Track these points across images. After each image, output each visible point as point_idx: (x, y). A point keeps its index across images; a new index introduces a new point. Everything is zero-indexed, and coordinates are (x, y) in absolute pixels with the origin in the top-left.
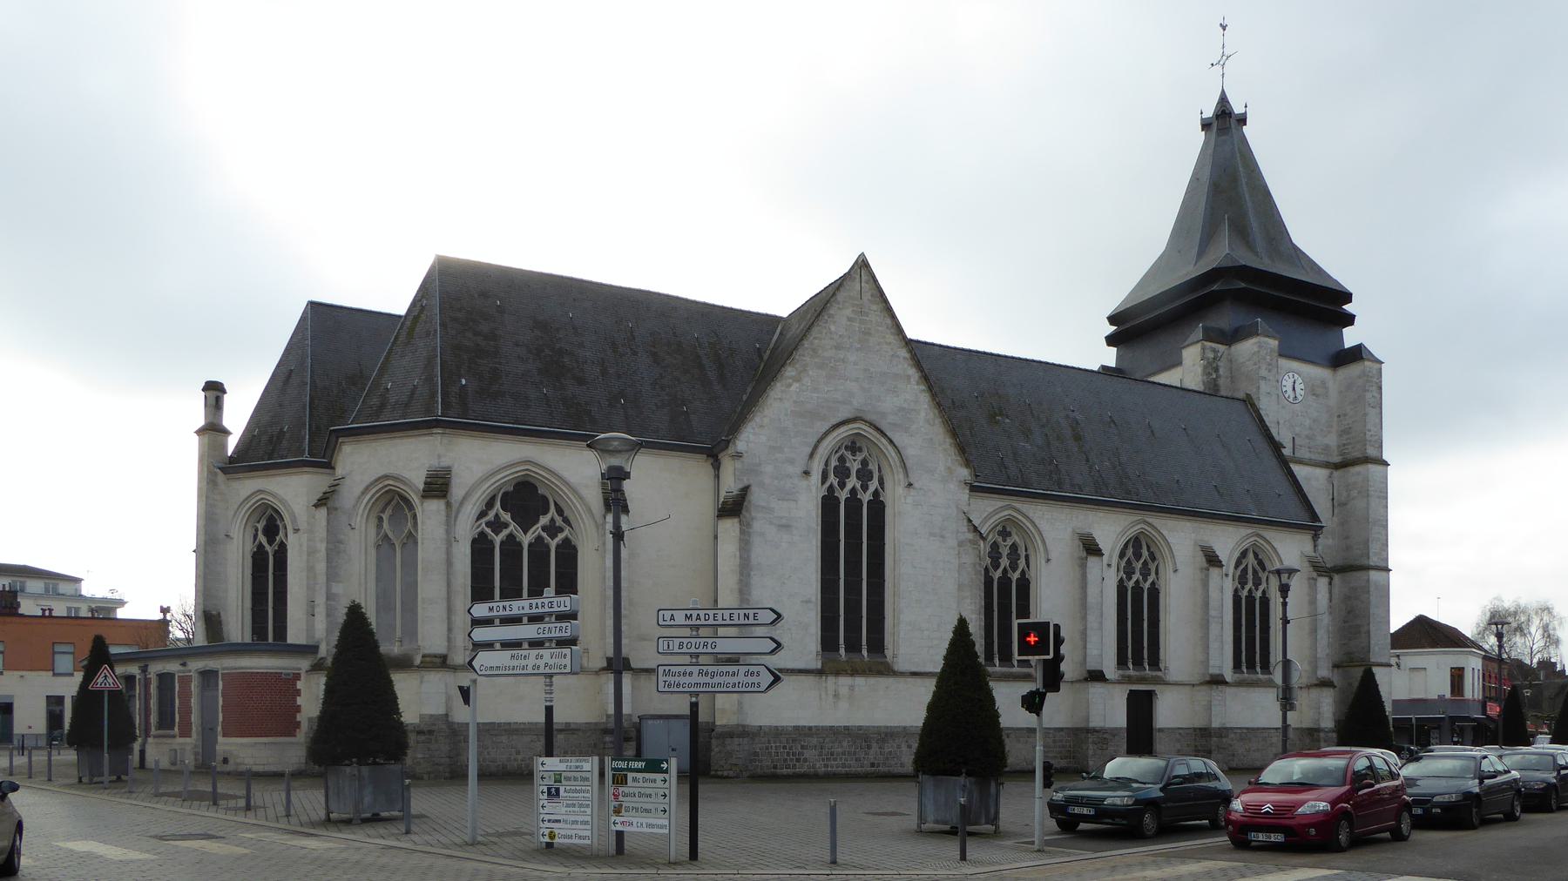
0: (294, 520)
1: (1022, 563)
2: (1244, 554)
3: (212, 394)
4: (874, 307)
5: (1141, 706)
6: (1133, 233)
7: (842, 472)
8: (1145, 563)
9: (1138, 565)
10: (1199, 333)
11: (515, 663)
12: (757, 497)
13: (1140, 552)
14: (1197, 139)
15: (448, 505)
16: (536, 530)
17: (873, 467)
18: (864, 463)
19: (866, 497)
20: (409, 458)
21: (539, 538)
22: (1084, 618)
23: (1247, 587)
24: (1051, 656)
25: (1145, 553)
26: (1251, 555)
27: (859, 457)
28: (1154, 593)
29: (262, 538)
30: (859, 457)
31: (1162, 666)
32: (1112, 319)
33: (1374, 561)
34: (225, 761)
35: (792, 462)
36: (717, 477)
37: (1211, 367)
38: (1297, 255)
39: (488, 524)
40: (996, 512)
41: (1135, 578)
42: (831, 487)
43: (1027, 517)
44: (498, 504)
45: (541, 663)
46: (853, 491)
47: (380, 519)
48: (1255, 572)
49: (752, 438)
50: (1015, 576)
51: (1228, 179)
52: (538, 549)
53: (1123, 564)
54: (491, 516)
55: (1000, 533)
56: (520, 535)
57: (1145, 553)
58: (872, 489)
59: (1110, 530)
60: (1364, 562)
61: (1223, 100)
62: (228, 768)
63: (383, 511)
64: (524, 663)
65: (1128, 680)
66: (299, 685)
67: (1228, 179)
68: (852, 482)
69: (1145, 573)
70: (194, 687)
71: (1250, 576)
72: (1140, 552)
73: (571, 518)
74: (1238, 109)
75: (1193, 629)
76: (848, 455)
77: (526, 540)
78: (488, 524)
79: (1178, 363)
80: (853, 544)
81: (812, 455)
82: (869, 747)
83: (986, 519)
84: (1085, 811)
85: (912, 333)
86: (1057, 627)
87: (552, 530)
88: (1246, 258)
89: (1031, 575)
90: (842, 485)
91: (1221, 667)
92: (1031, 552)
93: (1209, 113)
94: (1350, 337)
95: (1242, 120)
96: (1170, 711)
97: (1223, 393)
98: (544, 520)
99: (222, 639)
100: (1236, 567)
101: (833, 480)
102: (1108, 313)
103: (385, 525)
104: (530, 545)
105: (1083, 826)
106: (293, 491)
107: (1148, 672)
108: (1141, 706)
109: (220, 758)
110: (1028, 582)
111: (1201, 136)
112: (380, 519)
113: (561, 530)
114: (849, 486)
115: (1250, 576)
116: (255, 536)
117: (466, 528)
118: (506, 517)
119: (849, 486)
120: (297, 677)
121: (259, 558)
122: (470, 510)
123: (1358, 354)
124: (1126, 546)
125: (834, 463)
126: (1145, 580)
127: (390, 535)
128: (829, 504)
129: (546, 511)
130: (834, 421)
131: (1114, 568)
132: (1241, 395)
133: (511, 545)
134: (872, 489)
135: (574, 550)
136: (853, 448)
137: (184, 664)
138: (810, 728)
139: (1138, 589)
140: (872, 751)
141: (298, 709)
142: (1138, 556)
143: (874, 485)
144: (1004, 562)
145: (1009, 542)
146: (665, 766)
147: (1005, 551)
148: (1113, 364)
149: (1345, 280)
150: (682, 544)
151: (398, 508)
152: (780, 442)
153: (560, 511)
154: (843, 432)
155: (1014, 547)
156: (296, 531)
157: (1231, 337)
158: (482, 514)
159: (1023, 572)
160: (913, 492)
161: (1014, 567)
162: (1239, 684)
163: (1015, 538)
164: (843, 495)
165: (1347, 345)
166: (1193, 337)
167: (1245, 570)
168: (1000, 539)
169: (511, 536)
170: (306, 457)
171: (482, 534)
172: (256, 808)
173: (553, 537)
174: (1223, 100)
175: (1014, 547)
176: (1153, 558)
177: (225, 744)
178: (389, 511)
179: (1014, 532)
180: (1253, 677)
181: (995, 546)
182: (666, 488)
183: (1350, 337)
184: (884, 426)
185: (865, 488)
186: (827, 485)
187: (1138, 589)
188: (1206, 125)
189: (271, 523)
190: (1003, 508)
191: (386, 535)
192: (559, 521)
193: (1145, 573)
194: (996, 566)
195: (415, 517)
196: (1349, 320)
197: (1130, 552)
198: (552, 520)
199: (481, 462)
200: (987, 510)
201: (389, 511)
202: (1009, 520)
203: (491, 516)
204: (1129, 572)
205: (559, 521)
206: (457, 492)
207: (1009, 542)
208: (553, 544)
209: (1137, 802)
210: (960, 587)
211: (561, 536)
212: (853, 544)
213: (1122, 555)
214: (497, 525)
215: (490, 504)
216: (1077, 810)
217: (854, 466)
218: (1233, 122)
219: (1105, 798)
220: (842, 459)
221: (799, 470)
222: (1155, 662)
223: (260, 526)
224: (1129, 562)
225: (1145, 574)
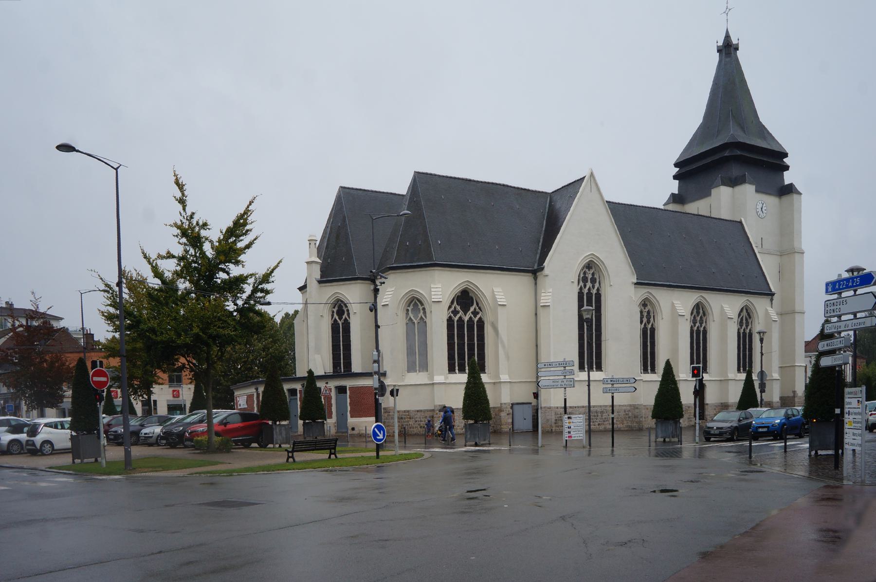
1: (652, 319)
6: (683, 120)
9: (698, 318)
10: (719, 180)
13: (699, 312)
14: (716, 57)
17: (596, 276)
18: (593, 274)
19: (594, 291)
25: (701, 311)
26: (745, 311)
27: (591, 272)
28: (705, 332)
29: (336, 316)
30: (591, 272)
32: (676, 165)
34: (353, 429)
38: (763, 131)
42: (581, 289)
47: (408, 310)
48: (746, 319)
50: (649, 326)
51: (730, 90)
54: (453, 308)
56: (463, 316)
57: (701, 311)
61: (727, 37)
62: (354, 432)
63: (409, 306)
67: (730, 90)
68: (589, 285)
70: (333, 394)
71: (744, 321)
77: (466, 319)
87: (475, 313)
89: (656, 325)
90: (585, 286)
93: (721, 43)
95: (737, 49)
98: (472, 309)
101: (581, 284)
106: (354, 294)
109: (350, 428)
111: (716, 56)
112: (408, 310)
113: (478, 313)
115: (744, 321)
116: (333, 316)
121: (335, 327)
123: (790, 190)
125: (582, 275)
133: (461, 320)
142: (698, 313)
147: (645, 314)
149: (787, 147)
150: (528, 321)
151: (416, 305)
153: (477, 304)
155: (649, 312)
158: (450, 307)
161: (649, 322)
163: (649, 307)
165: (787, 182)
167: (742, 319)
169: (460, 318)
171: (450, 317)
174: (727, 37)
175: (649, 312)
176: (704, 314)
177: (351, 421)
178: (411, 307)
188: (719, 51)
189: (340, 308)
192: (478, 310)
196: (787, 168)
201: (411, 307)
205: (478, 310)
208: (476, 320)
211: (478, 316)
213: (692, 314)
214: (455, 312)
215: (452, 302)
217: (590, 276)
218: (732, 49)
220: (585, 273)
223: (335, 310)
224: (694, 317)
225: (701, 324)
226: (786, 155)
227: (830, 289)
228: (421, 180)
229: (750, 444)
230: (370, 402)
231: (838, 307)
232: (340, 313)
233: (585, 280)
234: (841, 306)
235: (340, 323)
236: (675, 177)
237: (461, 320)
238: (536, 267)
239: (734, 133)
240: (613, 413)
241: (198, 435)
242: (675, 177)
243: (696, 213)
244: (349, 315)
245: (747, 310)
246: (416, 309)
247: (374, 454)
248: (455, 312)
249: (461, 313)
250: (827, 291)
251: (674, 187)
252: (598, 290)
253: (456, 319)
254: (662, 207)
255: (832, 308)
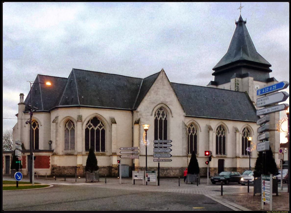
0: (40, 123)
1: (195, 132)
2: (244, 129)
3: (22, 96)
4: (165, 80)
5: (221, 163)
7: (159, 114)
8: (222, 131)
9: (221, 132)
11: (128, 157)
12: (142, 120)
13: (221, 129)
15: (82, 123)
16: (97, 127)
17: (165, 113)
18: (163, 112)
19: (163, 119)
20: (73, 113)
21: (98, 129)
22: (209, 143)
23: (245, 136)
24: (210, 156)
25: (222, 129)
26: (246, 129)
28: (224, 138)
30: (162, 111)
31: (226, 154)
32: (213, 69)
33: (276, 128)
35: (148, 112)
36: (133, 115)
37: (237, 85)
38: (258, 56)
39: (88, 126)
40: (190, 121)
41: (220, 135)
42: (156, 118)
43: (196, 122)
44: (90, 122)
45: (133, 157)
46: (161, 118)
47: (66, 125)
48: (247, 132)
49: (142, 108)
50: (194, 134)
52: (98, 131)
53: (217, 131)
54: (89, 124)
55: (190, 125)
56: (94, 128)
57: (222, 129)
58: (164, 118)
59: (214, 124)
60: (273, 129)
61: (241, 18)
63: (66, 123)
64: (130, 157)
65: (219, 157)
66: (50, 158)
68: (161, 116)
69: (222, 133)
70: (27, 158)
71: (246, 134)
72: (221, 129)
73: (104, 125)
74: (244, 20)
75: (233, 146)
76: (160, 111)
77: (95, 129)
78: (88, 126)
79: (229, 81)
80: (161, 130)
81: (153, 110)
82: (164, 171)
83: (187, 123)
84: (217, 180)
85: (171, 81)
86: (211, 151)
87: (100, 127)
88: (246, 57)
89: (197, 134)
90: (159, 117)
91: (239, 154)
92: (197, 130)
93: (237, 20)
94: (271, 75)
95: (245, 22)
96: (227, 164)
97: (240, 90)
98: (99, 125)
99: (38, 149)
100: (243, 131)
101: (157, 116)
102: (212, 68)
103: (67, 126)
104: (96, 130)
105: (217, 183)
106: (40, 118)
107: (223, 155)
108: (221, 163)
110: (196, 136)
111: (236, 25)
113: (102, 127)
114: (160, 117)
115: (246, 134)
117: (84, 128)
118: (92, 124)
119: (160, 117)
120: (50, 157)
121: (31, 131)
122: (85, 123)
124: (218, 128)
125: (157, 112)
126: (222, 135)
127: (68, 128)
128: (156, 121)
129: (99, 123)
130: (157, 104)
131: (215, 133)
132: (244, 91)
133: (93, 130)
134: (164, 118)
135: (104, 131)
136: (161, 109)
137: (24, 154)
138: (152, 167)
139: (220, 137)
140: (165, 172)
141: (50, 163)
142: (220, 129)
143: (165, 117)
144: (191, 132)
145: (192, 127)
146: (155, 172)
147: (192, 129)
148: (213, 80)
149: (270, 62)
151: (69, 123)
152: (146, 109)
153: (102, 123)
154: (159, 106)
155: (193, 129)
156: (41, 125)
157: (243, 76)
158: (87, 124)
159: (195, 134)
160: (173, 118)
161: (193, 133)
162: (244, 158)
163: (194, 126)
164: (159, 119)
165: (270, 77)
166: (233, 76)
167: (245, 132)
168: (190, 127)
169: (93, 128)
170: (43, 110)
171: (87, 128)
172: (66, 181)
173: (100, 128)
174: (241, 18)
175: (193, 129)
176: (224, 130)
179: (193, 125)
180: (247, 156)
181: (189, 128)
182: (121, 117)
183: (271, 75)
184: (167, 104)
185: (163, 117)
186: (156, 117)
187: (220, 137)
188: (237, 23)
189: (34, 124)
190: (191, 120)
191: (67, 128)
192: (102, 125)
193: (222, 133)
194: (189, 132)
195: (74, 125)
196: (271, 71)
197: (219, 129)
198: (100, 125)
199: (87, 114)
200: (188, 121)
202: (193, 123)
203: (89, 124)
204: (219, 133)
205: (102, 125)
206: (83, 120)
207: (192, 127)
208: (101, 130)
209: (225, 179)
210: (183, 138)
211: (102, 128)
212: (161, 130)
213: (217, 129)
214: (90, 126)
215: (88, 122)
216: (215, 180)
217: (161, 113)
218: (243, 23)
219: (220, 178)
220: (158, 112)
221: (150, 114)
222: (224, 153)
224: (219, 131)
226: (270, 66)
227: (259, 93)
228: (75, 71)
229: (248, 187)
230: (43, 162)
231: (264, 101)
232: (34, 125)
233: (159, 114)
234: (265, 101)
235: (34, 129)
236: (213, 74)
237: (93, 130)
238: (133, 108)
239: (242, 56)
240: (19, 145)
241: (221, 199)
242: (213, 74)
243: (223, 88)
244: (38, 126)
245: (247, 129)
246: (69, 125)
247: (15, 185)
248: (90, 126)
249: (93, 126)
250: (258, 94)
251: (213, 79)
252: (165, 119)
253: (90, 129)
254: (206, 86)
255: (260, 102)
